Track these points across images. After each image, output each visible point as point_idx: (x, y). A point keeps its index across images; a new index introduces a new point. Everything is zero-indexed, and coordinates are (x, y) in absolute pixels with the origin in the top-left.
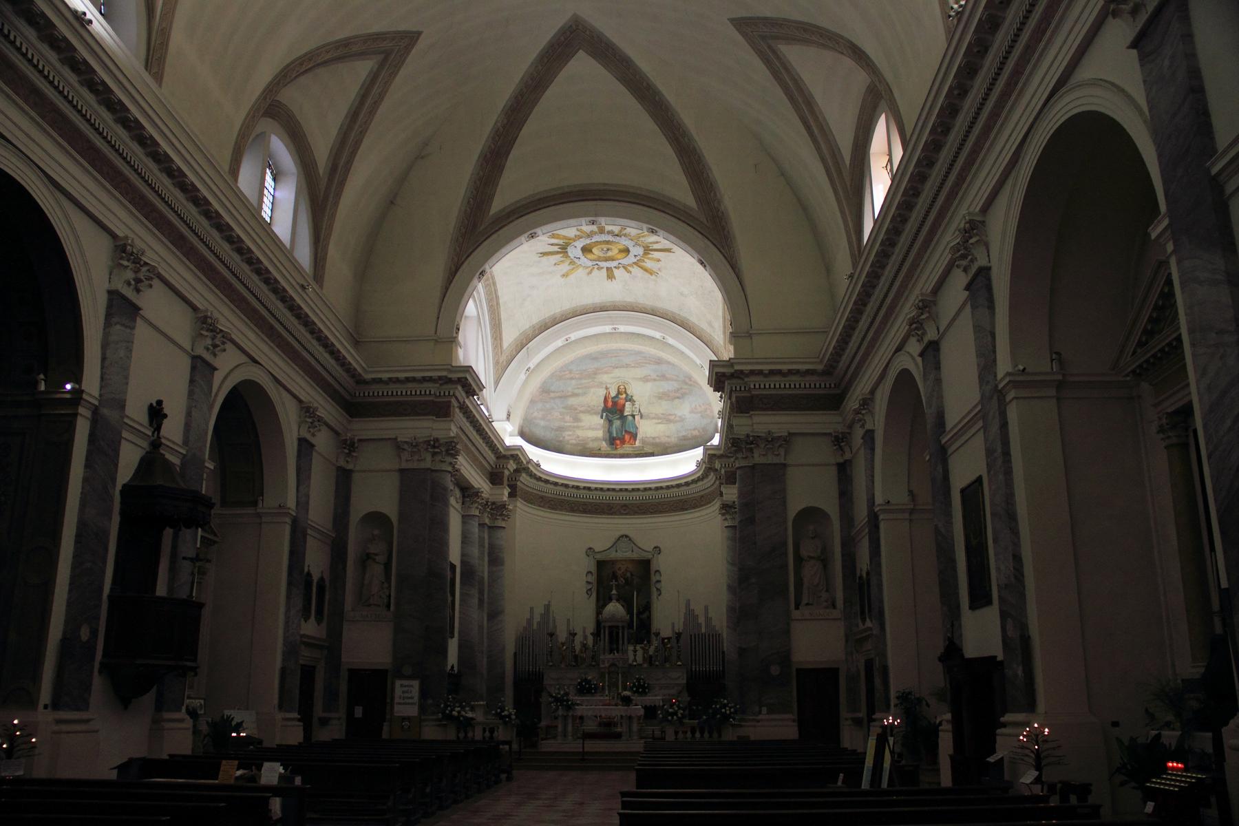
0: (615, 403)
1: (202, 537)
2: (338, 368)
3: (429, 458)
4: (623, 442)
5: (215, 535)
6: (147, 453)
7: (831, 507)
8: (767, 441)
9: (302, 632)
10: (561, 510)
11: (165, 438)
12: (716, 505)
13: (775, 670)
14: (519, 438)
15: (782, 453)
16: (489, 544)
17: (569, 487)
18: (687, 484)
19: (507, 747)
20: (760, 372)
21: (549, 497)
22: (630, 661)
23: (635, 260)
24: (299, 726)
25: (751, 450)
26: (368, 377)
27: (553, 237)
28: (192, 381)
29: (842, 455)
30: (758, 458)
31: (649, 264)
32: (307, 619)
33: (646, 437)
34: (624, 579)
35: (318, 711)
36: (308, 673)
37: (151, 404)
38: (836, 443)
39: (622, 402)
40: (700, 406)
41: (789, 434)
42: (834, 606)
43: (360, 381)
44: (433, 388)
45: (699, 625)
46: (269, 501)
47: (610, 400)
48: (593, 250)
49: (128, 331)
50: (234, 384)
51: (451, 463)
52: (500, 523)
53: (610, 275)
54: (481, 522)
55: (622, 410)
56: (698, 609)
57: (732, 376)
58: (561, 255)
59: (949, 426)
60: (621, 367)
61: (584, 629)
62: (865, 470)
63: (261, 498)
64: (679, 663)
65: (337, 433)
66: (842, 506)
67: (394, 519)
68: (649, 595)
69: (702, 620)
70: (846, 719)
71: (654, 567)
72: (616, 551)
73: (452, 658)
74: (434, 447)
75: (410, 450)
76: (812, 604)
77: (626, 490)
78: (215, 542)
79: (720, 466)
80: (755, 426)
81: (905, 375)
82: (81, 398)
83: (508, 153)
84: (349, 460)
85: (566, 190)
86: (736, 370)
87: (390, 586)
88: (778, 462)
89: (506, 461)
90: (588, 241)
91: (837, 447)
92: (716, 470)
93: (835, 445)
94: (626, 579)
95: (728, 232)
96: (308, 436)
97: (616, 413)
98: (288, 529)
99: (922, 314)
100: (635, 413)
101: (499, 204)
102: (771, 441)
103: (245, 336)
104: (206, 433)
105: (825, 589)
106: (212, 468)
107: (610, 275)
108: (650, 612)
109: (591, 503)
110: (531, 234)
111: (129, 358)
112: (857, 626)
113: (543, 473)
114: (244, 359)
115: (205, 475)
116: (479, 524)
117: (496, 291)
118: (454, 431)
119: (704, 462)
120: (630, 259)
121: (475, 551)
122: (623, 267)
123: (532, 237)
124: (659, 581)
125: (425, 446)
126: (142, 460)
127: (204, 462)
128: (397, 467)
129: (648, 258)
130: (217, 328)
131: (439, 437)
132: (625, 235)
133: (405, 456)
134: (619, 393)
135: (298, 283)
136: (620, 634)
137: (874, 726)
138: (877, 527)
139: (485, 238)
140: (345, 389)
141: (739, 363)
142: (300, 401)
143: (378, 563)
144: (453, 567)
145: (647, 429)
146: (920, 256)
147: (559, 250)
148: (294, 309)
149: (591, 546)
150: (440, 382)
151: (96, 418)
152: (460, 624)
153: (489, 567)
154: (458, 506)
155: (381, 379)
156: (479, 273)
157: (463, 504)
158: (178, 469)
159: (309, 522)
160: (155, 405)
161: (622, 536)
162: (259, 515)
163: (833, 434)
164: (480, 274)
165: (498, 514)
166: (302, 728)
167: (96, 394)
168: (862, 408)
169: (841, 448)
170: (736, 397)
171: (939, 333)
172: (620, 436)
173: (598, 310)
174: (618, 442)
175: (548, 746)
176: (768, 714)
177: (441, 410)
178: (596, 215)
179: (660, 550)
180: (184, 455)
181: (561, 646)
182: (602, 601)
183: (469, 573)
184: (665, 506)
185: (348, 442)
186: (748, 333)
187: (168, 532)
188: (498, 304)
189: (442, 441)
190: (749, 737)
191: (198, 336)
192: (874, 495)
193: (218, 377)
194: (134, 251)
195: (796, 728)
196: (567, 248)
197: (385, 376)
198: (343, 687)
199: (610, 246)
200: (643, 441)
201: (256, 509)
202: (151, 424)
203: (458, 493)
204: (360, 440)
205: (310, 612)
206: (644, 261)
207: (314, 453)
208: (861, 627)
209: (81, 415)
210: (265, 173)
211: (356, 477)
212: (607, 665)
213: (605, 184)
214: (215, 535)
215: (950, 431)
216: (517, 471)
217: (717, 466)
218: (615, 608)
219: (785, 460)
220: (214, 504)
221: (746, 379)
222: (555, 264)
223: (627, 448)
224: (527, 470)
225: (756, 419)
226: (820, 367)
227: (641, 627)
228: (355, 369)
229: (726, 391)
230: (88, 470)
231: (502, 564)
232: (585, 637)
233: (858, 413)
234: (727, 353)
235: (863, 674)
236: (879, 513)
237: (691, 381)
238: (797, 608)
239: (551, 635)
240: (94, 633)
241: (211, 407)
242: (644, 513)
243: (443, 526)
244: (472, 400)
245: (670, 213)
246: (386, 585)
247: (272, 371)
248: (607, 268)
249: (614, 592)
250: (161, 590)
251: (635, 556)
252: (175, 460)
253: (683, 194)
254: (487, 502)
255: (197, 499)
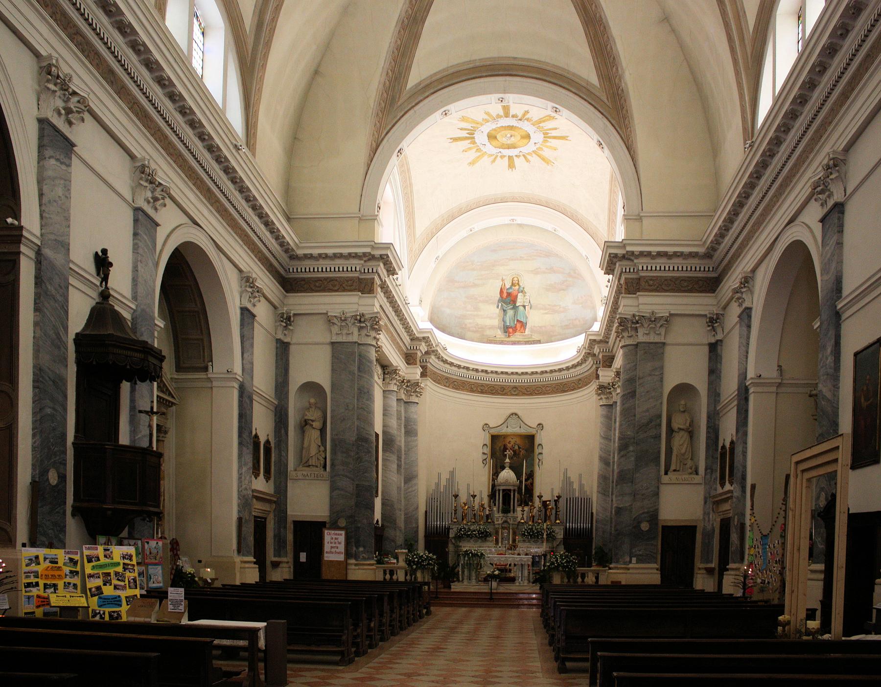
0: (509, 294)
1: (158, 396)
2: (273, 241)
3: (355, 331)
4: (515, 330)
5: (173, 397)
6: (97, 303)
7: (701, 384)
8: (651, 321)
9: (253, 487)
10: (462, 390)
11: (113, 289)
12: (593, 386)
13: (645, 526)
14: (429, 323)
15: (663, 333)
16: (405, 417)
17: (470, 370)
18: (568, 368)
19: (426, 587)
20: (649, 254)
21: (453, 378)
22: (519, 519)
23: (534, 148)
24: (255, 568)
25: (636, 329)
26: (300, 252)
27: (463, 120)
28: (135, 234)
29: (714, 336)
30: (641, 337)
31: (546, 153)
32: (257, 476)
33: (534, 326)
34: (513, 451)
35: (271, 556)
36: (260, 525)
37: (97, 253)
38: (710, 324)
39: (515, 293)
40: (582, 297)
41: (671, 315)
42: (697, 474)
43: (293, 257)
44: (356, 264)
45: (574, 490)
46: (218, 367)
47: (505, 291)
48: (498, 137)
49: (64, 167)
50: (177, 245)
51: (375, 338)
52: (414, 399)
53: (511, 165)
54: (399, 398)
55: (514, 301)
56: (574, 478)
57: (624, 257)
58: (469, 141)
59: (845, 292)
60: (515, 260)
61: (481, 492)
62: (739, 347)
63: (211, 363)
64: (558, 521)
65: (275, 307)
66: (710, 383)
67: (327, 387)
68: (533, 465)
69: (576, 486)
70: (700, 569)
71: (537, 441)
72: (507, 427)
73: (378, 515)
74: (360, 321)
75: (339, 324)
76: (678, 471)
77: (517, 373)
78: (173, 404)
79: (598, 350)
80: (641, 306)
81: (798, 249)
82: (22, 235)
83: (423, 21)
84: (286, 333)
85: (478, 64)
86: (627, 251)
87: (326, 449)
88: (659, 341)
89: (419, 343)
90: (494, 126)
91: (711, 328)
92: (595, 355)
93: (709, 326)
94: (514, 451)
95: (627, 111)
96: (249, 306)
97: (510, 303)
98: (236, 394)
99: (831, 173)
100: (525, 304)
101: (417, 74)
102: (653, 321)
103: (185, 195)
104: (154, 290)
105: (690, 458)
106: (162, 326)
107: (511, 165)
108: (533, 479)
109: (487, 385)
110: (445, 111)
111: (68, 198)
112: (716, 490)
113: (449, 356)
114: (185, 220)
115: (156, 334)
116: (397, 400)
117: (410, 178)
118: (377, 309)
119: (585, 348)
120: (530, 148)
121: (393, 422)
122: (524, 155)
123: (446, 114)
124: (541, 453)
125: (353, 321)
126: (93, 311)
127: (153, 319)
128: (328, 340)
129: (547, 147)
130: (156, 180)
131: (364, 312)
132: (528, 120)
133: (335, 329)
134: (513, 284)
135: (232, 143)
136: (512, 496)
137: (727, 575)
138: (747, 399)
139: (403, 113)
140: (279, 263)
141: (629, 244)
142: (240, 271)
143: (314, 428)
144: (377, 435)
145: (535, 319)
146: (834, 112)
147: (468, 136)
148: (228, 170)
149: (487, 423)
150: (364, 259)
151: (39, 259)
152: (383, 486)
153: (405, 436)
154: (380, 382)
155: (311, 255)
156: (397, 151)
157: (384, 380)
158: (130, 324)
159: (254, 389)
160: (100, 254)
161: (512, 414)
162: (209, 380)
163: (708, 316)
164: (399, 152)
165: (413, 391)
166: (258, 569)
167: (37, 232)
168: (742, 286)
169: (714, 329)
170: (626, 279)
171: (845, 195)
172: (512, 324)
173: (499, 201)
174: (511, 330)
175: (456, 587)
176: (637, 563)
177: (365, 286)
178: (505, 92)
179: (543, 427)
180: (134, 310)
181: (463, 505)
182: (498, 468)
183: (389, 442)
184: (548, 389)
185: (285, 316)
186: (639, 215)
187: (125, 386)
188: (411, 192)
189: (367, 317)
190: (620, 582)
191: (136, 188)
192: (746, 369)
193: (161, 234)
194: (61, 75)
195: (660, 576)
196: (474, 134)
197: (316, 252)
198: (290, 537)
199: (513, 132)
200: (532, 330)
201: (207, 374)
202: (98, 274)
203: (379, 370)
204: (295, 315)
205: (259, 470)
206: (542, 149)
207: (256, 324)
208: (720, 490)
209: (24, 254)
210: (193, 23)
211: (292, 348)
212: (500, 522)
213: (515, 58)
214: (173, 397)
215: (845, 298)
216: (427, 353)
217: (596, 350)
218: (507, 475)
219: (665, 339)
220: (164, 357)
221: (635, 261)
222: (463, 151)
223: (517, 336)
224: (435, 352)
225: (642, 300)
226: (701, 250)
227: (526, 493)
228: (288, 243)
229: (615, 272)
230: (38, 314)
231: (416, 435)
232: (482, 499)
233: (737, 292)
234: (619, 235)
235: (717, 531)
236: (749, 387)
237: (575, 273)
238: (666, 473)
239: (456, 496)
240: (62, 478)
241: (157, 264)
242: (531, 394)
243: (370, 397)
244: (392, 279)
245: (573, 90)
246: (322, 448)
247: (212, 236)
248: (509, 156)
249: (507, 460)
250: (124, 439)
251: (524, 431)
252: (127, 315)
253: (588, 72)
254: (404, 380)
255: (146, 349)
